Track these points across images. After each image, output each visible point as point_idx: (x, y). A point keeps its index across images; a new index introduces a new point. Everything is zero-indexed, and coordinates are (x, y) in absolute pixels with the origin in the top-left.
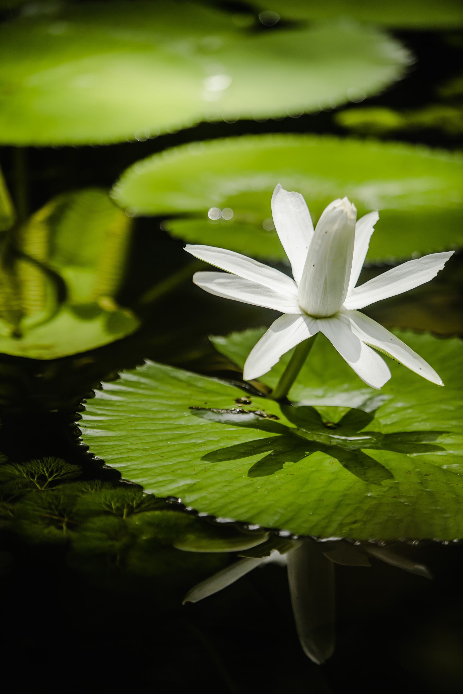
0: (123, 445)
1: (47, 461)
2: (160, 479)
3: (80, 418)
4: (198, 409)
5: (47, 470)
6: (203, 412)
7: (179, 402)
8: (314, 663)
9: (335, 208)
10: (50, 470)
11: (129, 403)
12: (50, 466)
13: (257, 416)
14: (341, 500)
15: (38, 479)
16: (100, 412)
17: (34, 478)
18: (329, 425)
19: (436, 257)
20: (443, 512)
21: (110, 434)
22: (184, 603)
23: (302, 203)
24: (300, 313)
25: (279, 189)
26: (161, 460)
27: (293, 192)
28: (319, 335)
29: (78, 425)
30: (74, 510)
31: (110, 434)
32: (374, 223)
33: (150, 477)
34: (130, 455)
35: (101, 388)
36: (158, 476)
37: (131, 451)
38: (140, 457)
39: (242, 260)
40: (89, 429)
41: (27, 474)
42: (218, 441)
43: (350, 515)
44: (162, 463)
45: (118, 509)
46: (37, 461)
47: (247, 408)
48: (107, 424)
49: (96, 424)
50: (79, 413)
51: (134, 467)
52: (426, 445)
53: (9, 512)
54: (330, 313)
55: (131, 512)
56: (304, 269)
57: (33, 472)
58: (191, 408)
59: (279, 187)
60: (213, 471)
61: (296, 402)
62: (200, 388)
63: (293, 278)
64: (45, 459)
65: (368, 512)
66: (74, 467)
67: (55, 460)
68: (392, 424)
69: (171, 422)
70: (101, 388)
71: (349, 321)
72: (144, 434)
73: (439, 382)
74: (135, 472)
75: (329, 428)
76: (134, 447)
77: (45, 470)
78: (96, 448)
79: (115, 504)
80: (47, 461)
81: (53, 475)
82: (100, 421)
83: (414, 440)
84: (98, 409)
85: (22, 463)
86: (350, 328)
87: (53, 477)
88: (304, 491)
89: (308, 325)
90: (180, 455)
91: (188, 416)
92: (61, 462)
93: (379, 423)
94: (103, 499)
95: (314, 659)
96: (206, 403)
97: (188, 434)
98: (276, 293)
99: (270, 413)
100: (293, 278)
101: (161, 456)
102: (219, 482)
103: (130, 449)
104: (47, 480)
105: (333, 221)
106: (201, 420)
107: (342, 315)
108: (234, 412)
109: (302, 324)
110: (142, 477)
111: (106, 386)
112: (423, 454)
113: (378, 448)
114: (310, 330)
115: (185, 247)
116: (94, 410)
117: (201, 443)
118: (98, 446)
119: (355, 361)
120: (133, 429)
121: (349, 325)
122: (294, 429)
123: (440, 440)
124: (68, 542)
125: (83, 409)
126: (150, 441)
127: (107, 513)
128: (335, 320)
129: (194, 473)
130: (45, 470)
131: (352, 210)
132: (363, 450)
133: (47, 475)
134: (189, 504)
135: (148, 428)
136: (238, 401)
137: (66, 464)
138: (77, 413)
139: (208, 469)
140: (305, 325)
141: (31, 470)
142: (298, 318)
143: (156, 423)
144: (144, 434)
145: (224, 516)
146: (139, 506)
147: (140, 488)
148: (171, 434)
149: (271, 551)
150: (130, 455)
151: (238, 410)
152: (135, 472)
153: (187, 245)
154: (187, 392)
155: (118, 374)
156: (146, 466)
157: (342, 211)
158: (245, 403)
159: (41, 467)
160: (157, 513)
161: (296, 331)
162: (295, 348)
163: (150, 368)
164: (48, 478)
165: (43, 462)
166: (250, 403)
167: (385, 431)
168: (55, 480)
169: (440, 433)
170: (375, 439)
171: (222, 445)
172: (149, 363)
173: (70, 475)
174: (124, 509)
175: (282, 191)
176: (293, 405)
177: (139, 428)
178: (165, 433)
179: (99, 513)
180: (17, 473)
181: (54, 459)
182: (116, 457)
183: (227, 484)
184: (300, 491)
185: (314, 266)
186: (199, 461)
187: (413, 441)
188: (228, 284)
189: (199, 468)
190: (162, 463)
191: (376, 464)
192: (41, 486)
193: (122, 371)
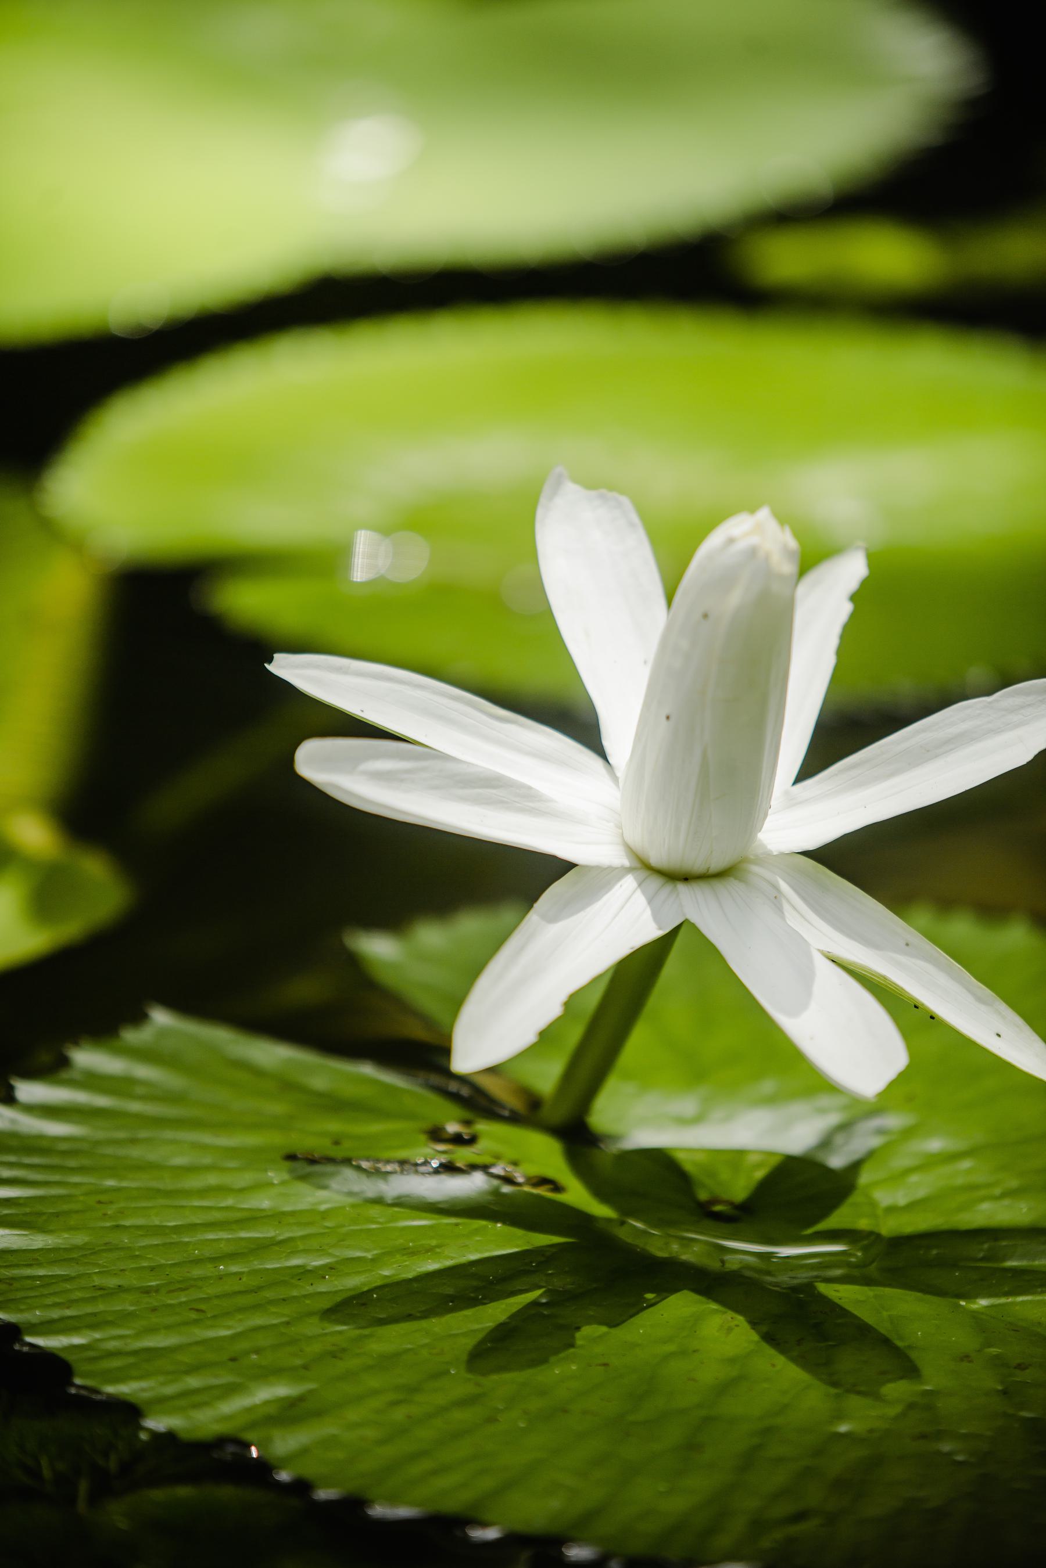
0: (79, 1276)
2: (193, 1382)
6: (329, 1168)
13: (496, 1182)
18: (718, 1208)
21: (38, 1241)
24: (627, 863)
31: (38, 1241)
33: (161, 1378)
47: (463, 1155)
48: (28, 1210)
51: (112, 1345)
52: (1017, 1273)
54: (716, 864)
58: (291, 1157)
69: (229, 1202)
71: (776, 887)
74: (116, 1363)
75: (718, 1217)
76: (112, 1282)
86: (780, 910)
89: (650, 902)
90: (256, 1307)
91: (283, 1183)
93: (873, 1204)
97: (281, 1238)
100: (601, 753)
102: (375, 1393)
105: (725, 580)
106: (322, 1194)
107: (755, 869)
113: (867, 1281)
114: (656, 916)
115: (270, 660)
121: (776, 899)
122: (609, 1220)
126: (163, 1262)
128: (729, 888)
129: (298, 1362)
135: (156, 1221)
136: (436, 1135)
139: (344, 1350)
140: (640, 900)
145: (393, 1499)
148: (228, 1240)
151: (435, 1164)
152: (116, 1363)
154: (277, 1108)
157: (752, 552)
160: (184, 1492)
163: (164, 1033)
166: (472, 1140)
167: (889, 1227)
170: (859, 1254)
171: (386, 1273)
172: (161, 1017)
175: (571, 489)
182: (55, 1314)
185: (668, 718)
189: (316, 1348)
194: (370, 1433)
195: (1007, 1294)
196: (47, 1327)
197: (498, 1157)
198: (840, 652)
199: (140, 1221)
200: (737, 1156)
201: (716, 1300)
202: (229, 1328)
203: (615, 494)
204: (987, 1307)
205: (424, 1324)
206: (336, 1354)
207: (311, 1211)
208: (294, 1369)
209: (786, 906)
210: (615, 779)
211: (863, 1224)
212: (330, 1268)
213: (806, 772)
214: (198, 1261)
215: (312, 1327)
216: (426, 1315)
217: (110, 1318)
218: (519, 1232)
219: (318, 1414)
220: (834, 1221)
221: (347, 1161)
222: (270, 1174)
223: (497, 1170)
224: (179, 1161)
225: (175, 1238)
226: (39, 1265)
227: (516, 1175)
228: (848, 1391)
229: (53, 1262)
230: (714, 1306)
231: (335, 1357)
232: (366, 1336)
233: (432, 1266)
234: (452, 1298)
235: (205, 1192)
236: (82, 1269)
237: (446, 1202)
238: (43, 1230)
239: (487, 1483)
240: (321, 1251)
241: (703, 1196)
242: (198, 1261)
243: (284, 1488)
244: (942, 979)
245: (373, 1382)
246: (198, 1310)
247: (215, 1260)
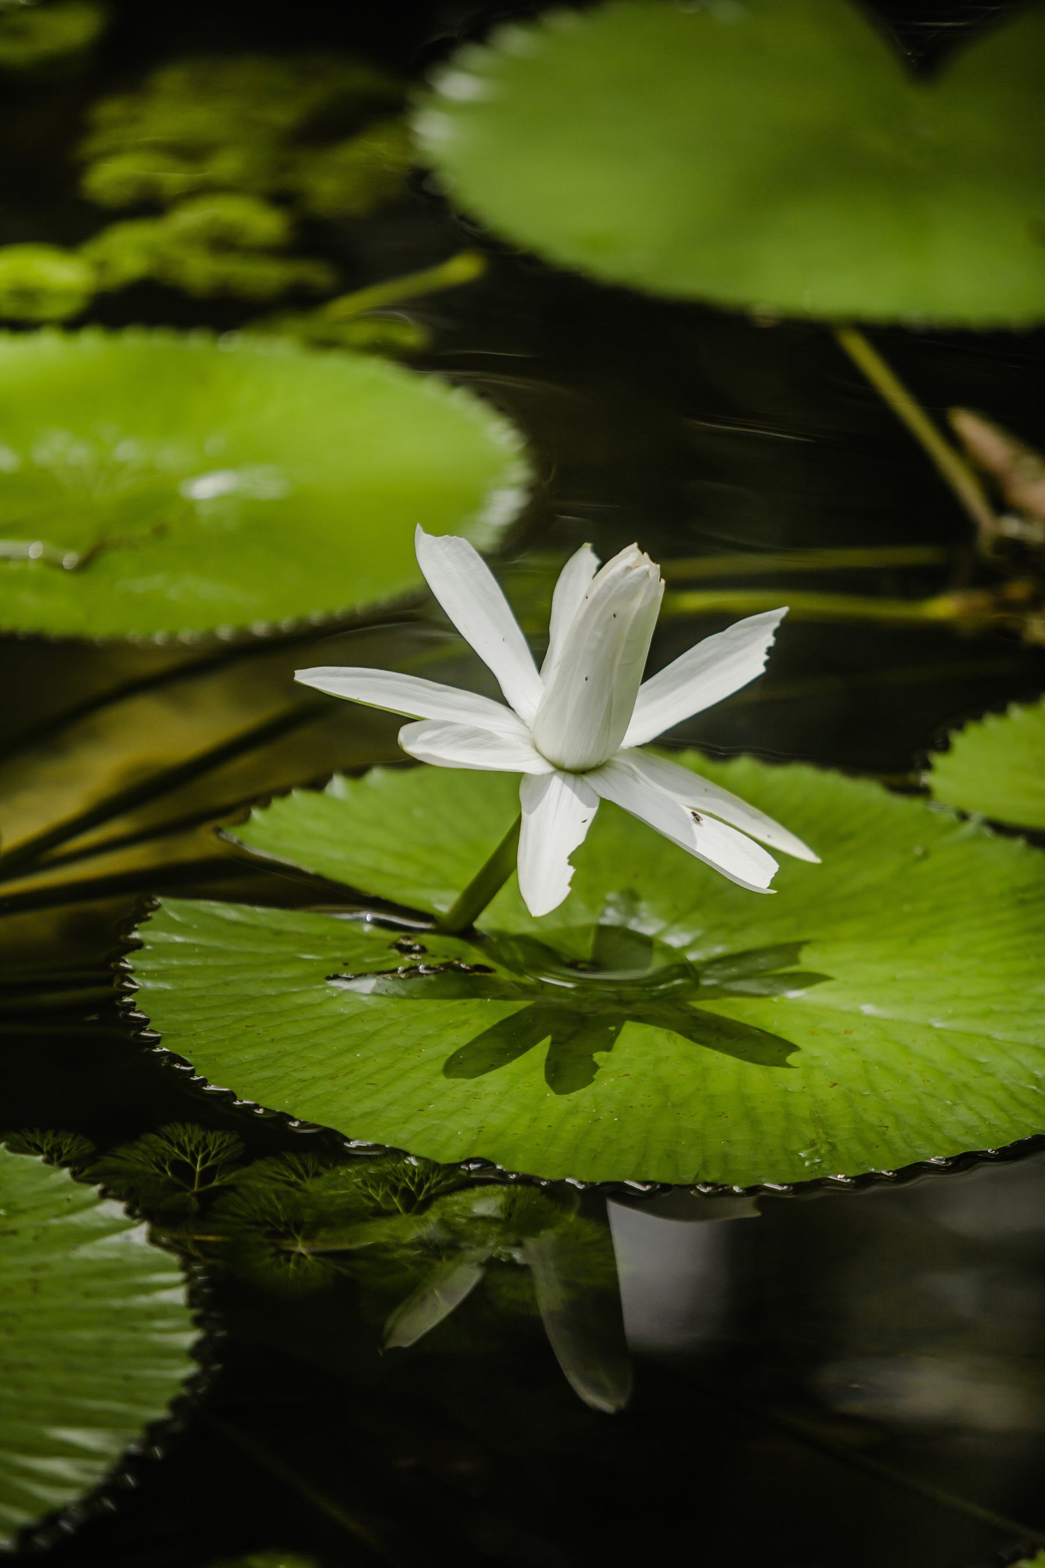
8: (601, 1414)
19: (754, 624)
24: (550, 769)
27: (447, 536)
39: (405, 684)
54: (593, 762)
63: (505, 703)
89: (574, 790)
95: (606, 1405)
100: (505, 703)
101: (372, 1084)
140: (568, 791)
142: (551, 779)
164: (193, 1166)
185: (586, 679)
186: (443, 1082)
209: (640, 781)
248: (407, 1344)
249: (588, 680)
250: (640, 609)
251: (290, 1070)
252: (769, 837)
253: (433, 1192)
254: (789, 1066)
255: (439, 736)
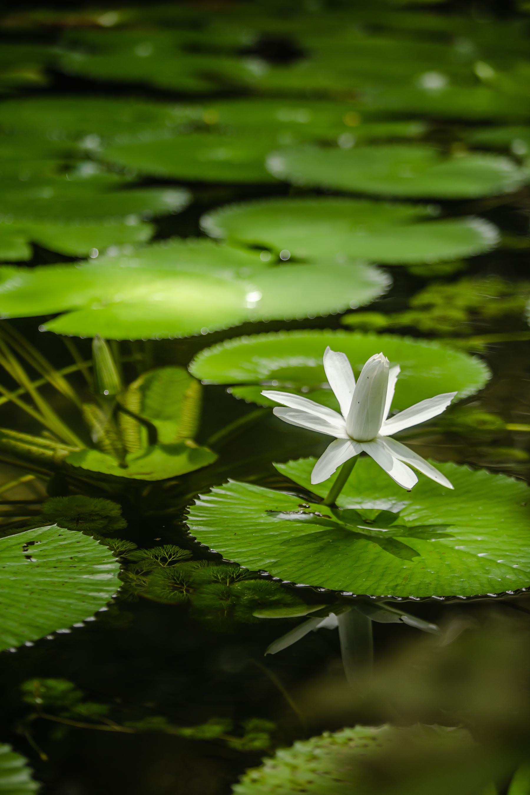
0: (221, 536)
1: (166, 547)
2: (251, 558)
3: (187, 519)
4: (271, 511)
5: (167, 553)
6: (276, 513)
7: (257, 508)
9: (374, 360)
10: (169, 554)
11: (221, 508)
12: (169, 551)
13: (316, 516)
14: (385, 571)
15: (160, 560)
16: (201, 515)
17: (158, 559)
18: (368, 521)
20: (459, 577)
21: (211, 529)
22: (265, 655)
23: (346, 360)
24: (348, 438)
25: (328, 351)
26: (250, 546)
28: (364, 454)
29: (186, 523)
30: (191, 580)
31: (211, 529)
32: (397, 374)
33: (244, 558)
34: (227, 543)
35: (199, 498)
36: (249, 557)
37: (227, 541)
38: (234, 544)
40: (194, 526)
41: (153, 557)
42: (289, 533)
43: (392, 580)
44: (251, 548)
45: (223, 579)
46: (159, 548)
47: (307, 510)
48: (206, 522)
49: (199, 523)
50: (186, 515)
51: (231, 551)
52: (440, 534)
53: (142, 582)
54: (370, 438)
55: (232, 581)
56: (351, 405)
57: (157, 555)
58: (267, 511)
59: (328, 348)
60: (288, 553)
61: (342, 507)
62: (271, 498)
64: (165, 546)
65: (405, 579)
66: (187, 552)
67: (172, 547)
68: (414, 520)
69: (254, 521)
70: (199, 498)
71: (383, 444)
72: (235, 529)
73: (451, 487)
74: (233, 555)
75: (368, 523)
76: (229, 538)
77: (165, 553)
78: (202, 538)
79: (220, 576)
80: (166, 547)
81: (171, 557)
82: (202, 521)
83: (431, 530)
84: (199, 513)
85: (148, 549)
86: (384, 449)
87: (172, 558)
88: (357, 565)
89: (354, 447)
90: (263, 543)
91: (265, 517)
92: (177, 548)
93: (404, 520)
94: (212, 573)
96: (277, 508)
97: (267, 528)
98: (330, 423)
99: (324, 514)
100: (341, 413)
102: (294, 561)
103: (226, 539)
104: (167, 561)
105: (373, 369)
106: (275, 519)
107: (378, 440)
108: (299, 513)
109: (350, 446)
110: (238, 558)
111: (202, 497)
112: (439, 540)
113: (405, 537)
114: (355, 450)
115: (262, 392)
116: (196, 514)
117: (277, 534)
118: (202, 537)
119: (390, 470)
120: (226, 525)
121: (383, 447)
122: (343, 525)
123: (449, 530)
124: (188, 603)
125: (188, 513)
126: (240, 533)
127: (216, 582)
128: (372, 444)
129: (275, 554)
130: (165, 553)
131: (387, 361)
132: (395, 538)
133: (167, 557)
134: (276, 575)
135: (237, 525)
136: (301, 506)
137: (180, 549)
138: (184, 515)
139: (285, 552)
140: (352, 447)
141: (155, 554)
143: (243, 522)
144: (235, 529)
145: (300, 583)
146: (238, 577)
147: (237, 565)
148: (254, 529)
149: (329, 614)
150: (227, 543)
151: (301, 512)
152: (233, 555)
153: (263, 391)
154: (262, 501)
155: (210, 489)
156: (239, 550)
157: (380, 362)
158: (305, 507)
159: (162, 552)
160: (252, 581)
161: (345, 451)
162: (343, 465)
163: (232, 484)
165: (164, 548)
166: (309, 507)
167: (409, 525)
168: (174, 560)
169: (448, 525)
170: (402, 531)
171: (293, 535)
172: (231, 481)
173: (184, 557)
174: (227, 579)
175: (331, 352)
176: (340, 509)
177: (230, 525)
178: (250, 528)
179: (210, 582)
180: (146, 556)
181: (172, 546)
182: (217, 544)
183: (300, 562)
184: (354, 566)
185: (359, 403)
187: (430, 531)
188: (297, 416)
189: (279, 551)
190: (251, 548)
191: (406, 547)
192: (163, 564)
193: (213, 487)
194: (294, 569)
195: (438, 538)
196: (213, 547)
197: (316, 511)
198: (395, 389)
199: (233, 525)
200: (371, 510)
201: (371, 541)
202: (258, 547)
203: (341, 353)
204: (434, 542)
205: (303, 546)
206: (284, 553)
207: (273, 523)
208: (274, 556)
209: (385, 448)
210: (344, 419)
211: (403, 524)
212: (279, 535)
213: (388, 418)
214: (248, 533)
215: (277, 547)
216: (303, 545)
217: (230, 545)
218: (323, 527)
219: (281, 565)
220: (396, 523)
221: (281, 512)
222: (262, 515)
223: (316, 513)
224: (241, 512)
225: (242, 528)
226: (211, 534)
227: (320, 514)
228: (404, 559)
229: (215, 533)
230: (371, 542)
231: (283, 553)
232: (290, 549)
233: (303, 534)
234: (309, 541)
235: (247, 519)
236: (222, 535)
237: (304, 520)
238: (211, 527)
239: (323, 579)
240: (276, 531)
241: (364, 519)
242: (248, 533)
243: (276, 581)
244: (423, 465)
245: (294, 558)
246: (250, 544)
247: (253, 533)
248: (273, 653)
249: (359, 403)
250: (376, 375)
251: (225, 535)
252: (436, 477)
253: (241, 579)
254: (413, 561)
255: (298, 415)
